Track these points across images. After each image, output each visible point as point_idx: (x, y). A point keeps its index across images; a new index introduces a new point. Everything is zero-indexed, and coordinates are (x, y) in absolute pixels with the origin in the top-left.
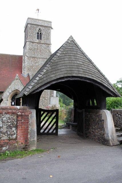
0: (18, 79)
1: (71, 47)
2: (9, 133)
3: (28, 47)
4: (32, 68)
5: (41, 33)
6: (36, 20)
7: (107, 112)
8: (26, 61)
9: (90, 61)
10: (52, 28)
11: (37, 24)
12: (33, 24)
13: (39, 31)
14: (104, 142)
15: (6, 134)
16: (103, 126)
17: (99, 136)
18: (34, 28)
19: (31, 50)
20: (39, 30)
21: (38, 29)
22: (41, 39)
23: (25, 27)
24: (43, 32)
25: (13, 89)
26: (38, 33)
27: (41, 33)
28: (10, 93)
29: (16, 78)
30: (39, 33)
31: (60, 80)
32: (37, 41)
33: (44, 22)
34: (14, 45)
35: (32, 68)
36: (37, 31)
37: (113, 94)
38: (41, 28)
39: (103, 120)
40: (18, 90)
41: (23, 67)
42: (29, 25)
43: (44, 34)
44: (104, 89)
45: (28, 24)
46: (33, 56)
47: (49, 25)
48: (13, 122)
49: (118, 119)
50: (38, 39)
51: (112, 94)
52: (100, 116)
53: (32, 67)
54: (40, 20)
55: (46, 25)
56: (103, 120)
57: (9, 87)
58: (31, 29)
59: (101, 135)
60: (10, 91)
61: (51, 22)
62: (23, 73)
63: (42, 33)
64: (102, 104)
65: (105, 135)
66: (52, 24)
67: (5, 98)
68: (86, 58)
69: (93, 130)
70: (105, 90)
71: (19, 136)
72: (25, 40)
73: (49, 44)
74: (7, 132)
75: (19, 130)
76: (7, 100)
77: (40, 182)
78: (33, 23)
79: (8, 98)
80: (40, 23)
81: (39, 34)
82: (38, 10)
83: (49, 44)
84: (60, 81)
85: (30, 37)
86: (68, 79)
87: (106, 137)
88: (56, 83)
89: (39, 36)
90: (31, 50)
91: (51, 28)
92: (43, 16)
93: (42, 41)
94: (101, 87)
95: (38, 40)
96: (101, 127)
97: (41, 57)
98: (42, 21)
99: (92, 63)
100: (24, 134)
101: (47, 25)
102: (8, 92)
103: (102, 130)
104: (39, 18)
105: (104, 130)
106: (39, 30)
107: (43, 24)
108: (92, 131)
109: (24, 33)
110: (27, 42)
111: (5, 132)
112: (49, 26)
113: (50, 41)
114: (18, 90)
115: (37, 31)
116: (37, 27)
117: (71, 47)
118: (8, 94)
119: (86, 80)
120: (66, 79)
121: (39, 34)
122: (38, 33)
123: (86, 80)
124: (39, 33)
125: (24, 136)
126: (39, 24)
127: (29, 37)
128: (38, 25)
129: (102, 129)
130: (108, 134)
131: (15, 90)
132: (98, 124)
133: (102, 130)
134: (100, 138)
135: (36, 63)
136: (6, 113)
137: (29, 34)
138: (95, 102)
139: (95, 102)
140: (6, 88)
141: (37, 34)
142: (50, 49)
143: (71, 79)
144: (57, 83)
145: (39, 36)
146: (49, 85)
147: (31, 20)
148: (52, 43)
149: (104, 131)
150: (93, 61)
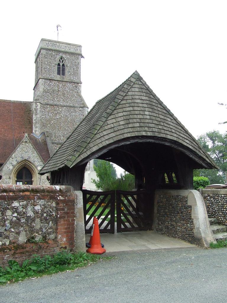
0: (28, 141)
1: (134, 91)
2: (44, 230)
3: (41, 88)
4: (50, 123)
5: (63, 65)
6: (55, 43)
7: (196, 193)
8: (38, 112)
9: (168, 112)
10: (83, 57)
11: (58, 49)
12: (50, 50)
13: (61, 61)
14: (194, 239)
15: (40, 233)
16: (191, 216)
17: (183, 232)
18: (51, 56)
20: (61, 59)
21: (58, 57)
22: (63, 74)
23: (37, 55)
24: (67, 63)
25: (19, 159)
26: (59, 65)
27: (63, 65)
29: (24, 141)
30: (61, 64)
31: (116, 144)
32: (58, 77)
33: (69, 46)
34: (17, 85)
37: (206, 164)
38: (64, 56)
39: (190, 207)
40: (28, 161)
41: (34, 122)
42: (43, 52)
43: (68, 65)
44: (191, 156)
45: (41, 49)
46: (51, 102)
47: (78, 52)
48: (50, 212)
49: (210, 205)
50: (59, 73)
51: (204, 164)
52: (184, 200)
53: (49, 121)
54: (63, 43)
55: (72, 50)
56: (190, 207)
57: (13, 155)
58: (46, 58)
59: (186, 230)
60: (15, 163)
61: (80, 46)
62: (34, 131)
63: (65, 65)
64: (185, 182)
65: (195, 231)
66: (83, 49)
67: (5, 174)
68: (162, 107)
69: (172, 223)
70: (194, 157)
71: (60, 236)
72: (36, 76)
73: (78, 83)
74: (41, 228)
75: (62, 225)
76: (10, 178)
77: (119, 301)
78: (50, 47)
79: (11, 174)
80: (63, 47)
81: (61, 67)
83: (78, 83)
84: (123, 144)
85: (46, 71)
86: (136, 141)
87: (195, 234)
88: (116, 148)
89: (61, 69)
90: (47, 92)
91: (80, 57)
92: (66, 37)
93: (67, 78)
94: (188, 153)
95: (59, 76)
96: (187, 218)
97: (65, 104)
98: (65, 45)
99: (172, 115)
100: (68, 232)
101: (73, 52)
102: (11, 163)
103: (189, 223)
104: (60, 40)
105: (192, 222)
106: (61, 59)
107: (67, 50)
108: (172, 225)
109: (34, 65)
110: (40, 80)
111: (38, 229)
112: (77, 52)
113: (79, 78)
114: (29, 160)
115: (58, 63)
116: (57, 55)
117: (134, 91)
118: (11, 167)
119: (163, 143)
120: (132, 141)
121: (61, 67)
122: (59, 65)
123: (163, 143)
124: (61, 64)
125: (67, 236)
126: (61, 49)
127: (43, 71)
128: (59, 52)
129: (189, 221)
130: (198, 228)
131: (23, 161)
132: (182, 213)
133: (189, 223)
134: (186, 236)
135: (56, 114)
136: (39, 198)
137: (44, 66)
138: (167, 180)
139: (167, 180)
140: (6, 156)
141: (57, 66)
142: (79, 92)
143: (141, 141)
144: (118, 147)
145: (61, 69)
146: (105, 151)
147: (48, 42)
149: (191, 223)
150: (172, 111)
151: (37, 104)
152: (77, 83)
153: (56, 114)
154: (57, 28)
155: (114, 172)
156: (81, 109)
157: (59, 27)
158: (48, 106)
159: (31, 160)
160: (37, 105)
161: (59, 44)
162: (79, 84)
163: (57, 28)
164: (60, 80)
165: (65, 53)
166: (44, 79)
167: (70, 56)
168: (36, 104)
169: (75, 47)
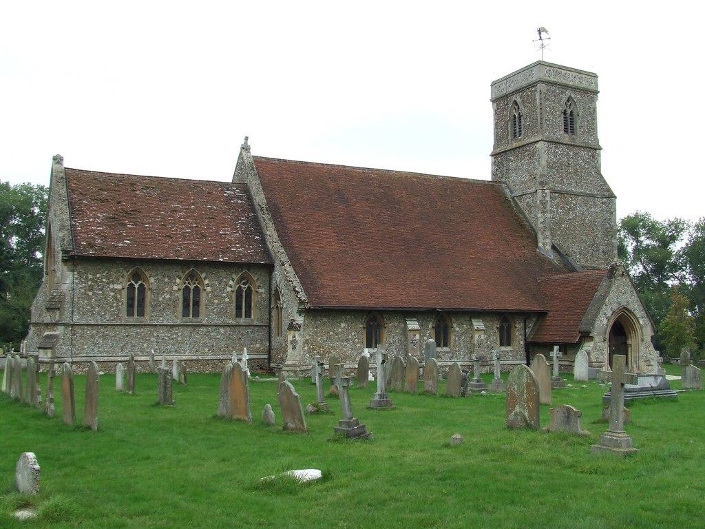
11: (564, 82)
19: (552, 168)
21: (565, 98)
25: (615, 306)
26: (565, 113)
28: (608, 319)
30: (569, 112)
32: (566, 138)
35: (559, 228)
36: (547, 111)
38: (573, 96)
50: (566, 131)
53: (559, 223)
60: (609, 313)
61: (595, 76)
62: (540, 245)
63: (575, 113)
73: (596, 149)
78: (552, 79)
82: (549, 38)
83: (596, 149)
85: (548, 126)
92: (515, 56)
98: (574, 74)
107: (577, 83)
113: (597, 140)
116: (562, 93)
118: (605, 321)
124: (569, 112)
128: (565, 87)
135: (569, 210)
147: (548, 68)
148: (601, 144)
151: (546, 191)
152: (595, 149)
153: (569, 210)
154: (540, 34)
155: (18, 244)
156: (604, 200)
157: (543, 34)
158: (557, 195)
159: (630, 307)
160: (546, 193)
161: (565, 72)
162: (598, 151)
163: (540, 34)
164: (570, 143)
165: (574, 89)
166: (548, 142)
167: (581, 95)
168: (543, 193)
169: (588, 77)
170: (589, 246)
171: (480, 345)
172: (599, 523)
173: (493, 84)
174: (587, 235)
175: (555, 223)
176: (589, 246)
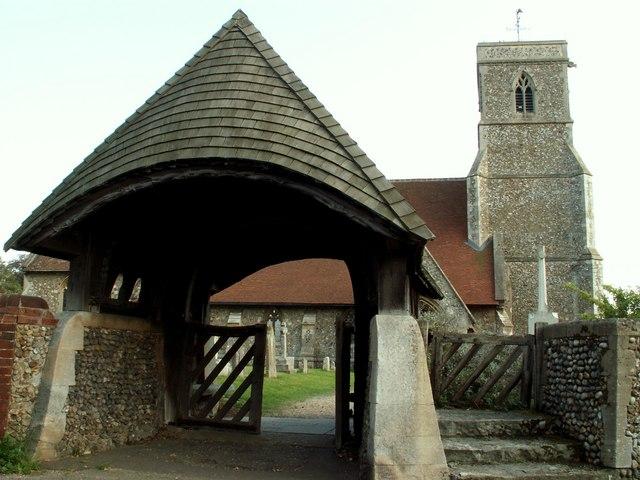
30: (524, 89)
35: (504, 217)
38: (528, 70)
61: (563, 43)
62: (470, 237)
73: (564, 124)
83: (564, 124)
107: (533, 56)
116: (512, 70)
124: (524, 89)
135: (518, 196)
148: (573, 116)
158: (500, 181)
165: (525, 62)
169: (550, 47)
170: (552, 234)
171: (308, 340)
172: (414, 478)
173: (480, 46)
174: (547, 222)
175: (498, 212)
176: (552, 234)
